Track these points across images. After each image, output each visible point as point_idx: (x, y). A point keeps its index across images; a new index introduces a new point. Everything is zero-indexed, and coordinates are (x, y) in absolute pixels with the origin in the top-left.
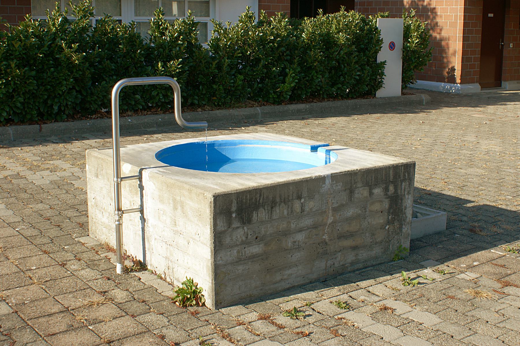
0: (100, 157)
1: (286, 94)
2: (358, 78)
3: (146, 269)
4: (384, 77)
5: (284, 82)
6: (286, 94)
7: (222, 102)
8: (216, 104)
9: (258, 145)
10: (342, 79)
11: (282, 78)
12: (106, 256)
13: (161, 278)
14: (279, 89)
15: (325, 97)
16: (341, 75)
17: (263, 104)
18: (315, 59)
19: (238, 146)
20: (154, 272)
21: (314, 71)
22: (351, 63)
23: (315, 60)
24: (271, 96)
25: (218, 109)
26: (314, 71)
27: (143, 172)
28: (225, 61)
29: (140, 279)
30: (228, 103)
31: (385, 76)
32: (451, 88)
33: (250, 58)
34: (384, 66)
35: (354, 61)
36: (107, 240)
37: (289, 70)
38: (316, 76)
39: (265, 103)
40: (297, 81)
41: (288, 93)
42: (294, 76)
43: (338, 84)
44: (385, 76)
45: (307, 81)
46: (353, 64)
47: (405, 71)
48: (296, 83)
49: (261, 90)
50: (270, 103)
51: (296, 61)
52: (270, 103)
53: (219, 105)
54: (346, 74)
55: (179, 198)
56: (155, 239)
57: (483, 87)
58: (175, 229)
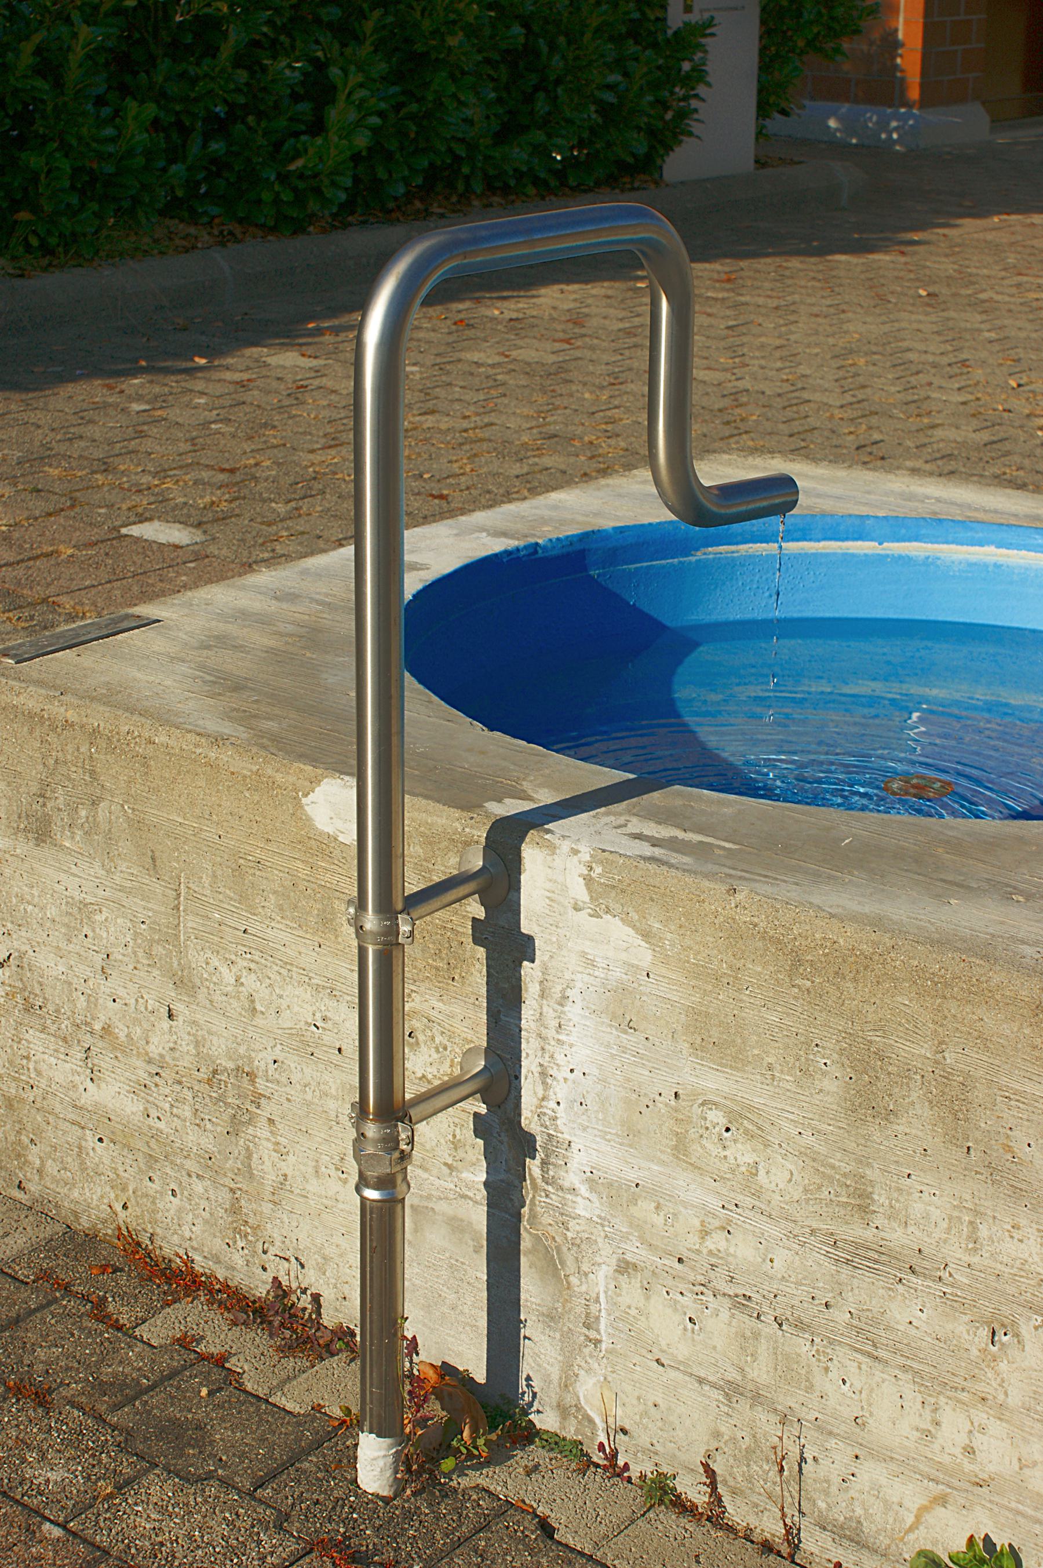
0: (71, 715)
1: (333, 184)
2: (610, 97)
3: (529, 1435)
4: (701, 90)
5: (317, 127)
6: (333, 184)
7: (61, 235)
8: (34, 242)
9: (801, 544)
10: (541, 105)
11: (305, 107)
12: (184, 1342)
13: (682, 1507)
14: (299, 163)
15: (478, 187)
16: (536, 88)
17: (231, 233)
18: (452, 17)
19: (699, 555)
20: (598, 1458)
21: (444, 74)
22: (583, 34)
23: (454, 22)
24: (267, 196)
25: (45, 269)
26: (444, 74)
27: (531, 855)
28: (75, 35)
29: (546, 1528)
30: (84, 235)
31: (709, 85)
32: (883, 125)
33: (167, 17)
34: (703, 41)
35: (595, 23)
36: (122, 1215)
37: (345, 71)
38: (454, 96)
39: (238, 231)
40: (375, 120)
41: (337, 178)
42: (363, 101)
43: (527, 128)
44: (709, 85)
45: (412, 117)
46: (588, 35)
47: (767, 63)
48: (375, 131)
49: (217, 166)
50: (263, 226)
51: (369, 26)
52: (263, 226)
53: (47, 250)
54: (558, 82)
55: (926, 1050)
56: (625, 1267)
57: (997, 122)
58: (856, 1231)
